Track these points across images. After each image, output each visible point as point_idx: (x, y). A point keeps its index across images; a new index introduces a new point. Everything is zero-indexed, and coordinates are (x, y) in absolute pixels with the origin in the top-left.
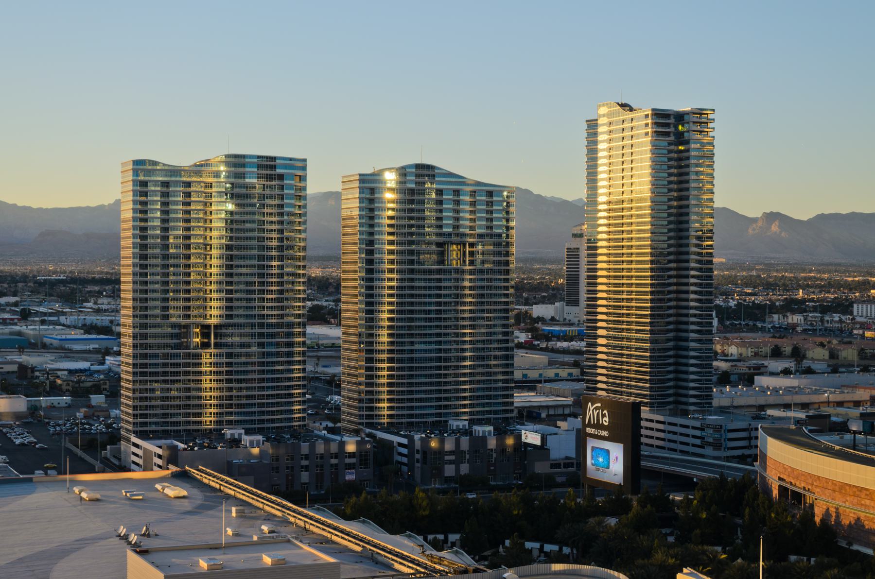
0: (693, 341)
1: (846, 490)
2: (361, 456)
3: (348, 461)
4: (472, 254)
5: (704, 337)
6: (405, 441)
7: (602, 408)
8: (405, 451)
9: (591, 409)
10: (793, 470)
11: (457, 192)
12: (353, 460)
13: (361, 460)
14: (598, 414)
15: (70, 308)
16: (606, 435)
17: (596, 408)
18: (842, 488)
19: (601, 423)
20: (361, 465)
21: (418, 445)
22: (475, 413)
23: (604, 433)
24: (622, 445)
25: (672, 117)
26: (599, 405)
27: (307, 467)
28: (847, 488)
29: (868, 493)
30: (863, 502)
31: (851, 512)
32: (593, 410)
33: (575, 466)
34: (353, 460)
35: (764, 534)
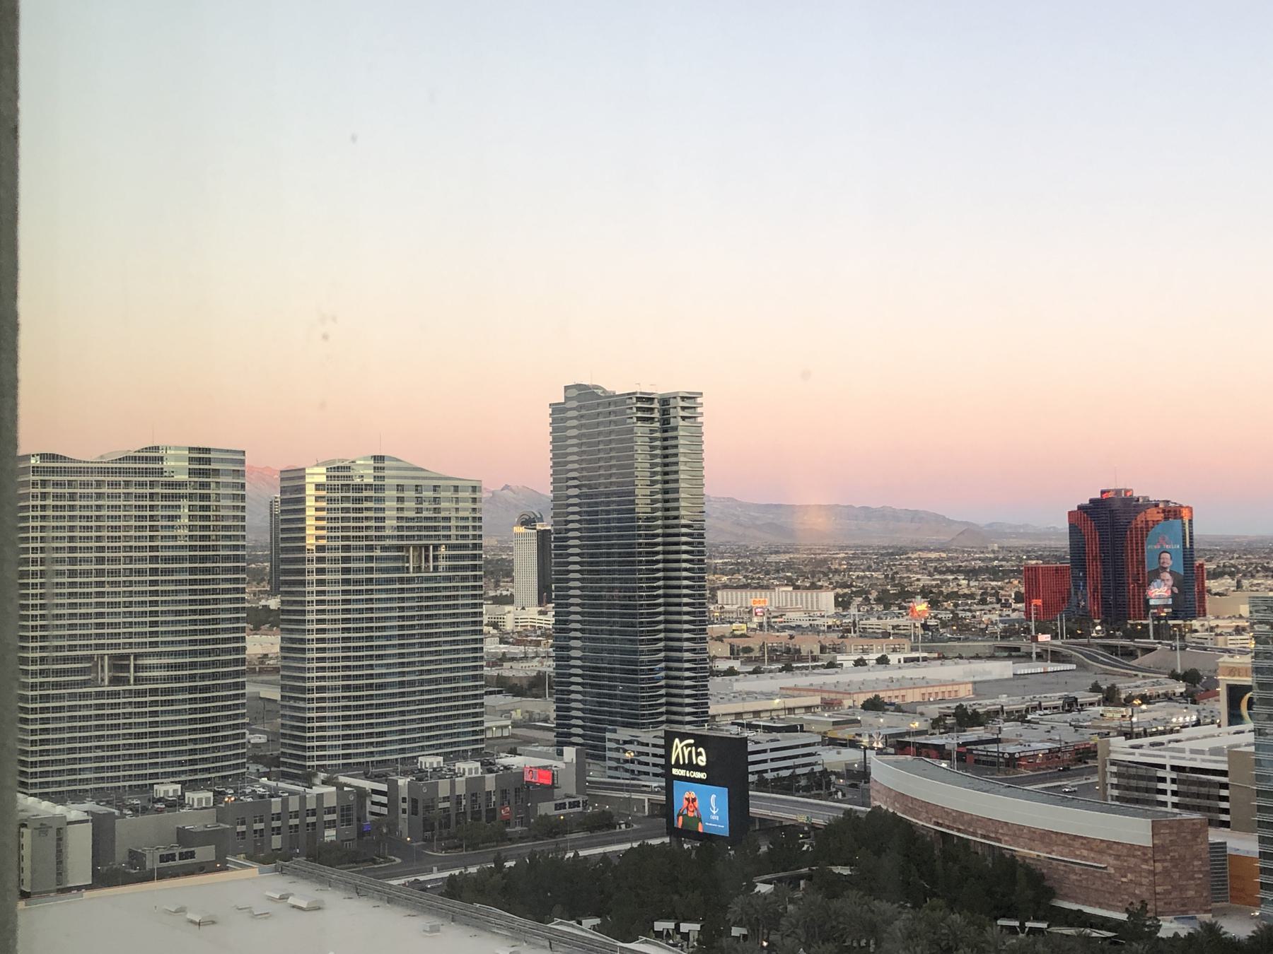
0: (687, 651)
1: (1051, 839)
2: (342, 810)
3: (327, 817)
4: (436, 558)
5: (698, 646)
6: (384, 787)
7: (696, 745)
8: (384, 800)
9: (680, 746)
10: (962, 814)
11: (417, 488)
12: (333, 817)
13: (342, 816)
14: (690, 753)
15: (1031, 771)
16: (703, 777)
17: (687, 746)
18: (1047, 838)
19: (695, 762)
20: (342, 821)
21: (404, 793)
22: (48, 686)
23: (702, 776)
24: (726, 790)
25: (656, 401)
26: (692, 741)
27: (279, 828)
28: (1053, 836)
29: (1085, 841)
30: (1078, 853)
31: (1060, 865)
32: (682, 748)
33: (581, 805)
34: (333, 817)
35: (674, 844)
